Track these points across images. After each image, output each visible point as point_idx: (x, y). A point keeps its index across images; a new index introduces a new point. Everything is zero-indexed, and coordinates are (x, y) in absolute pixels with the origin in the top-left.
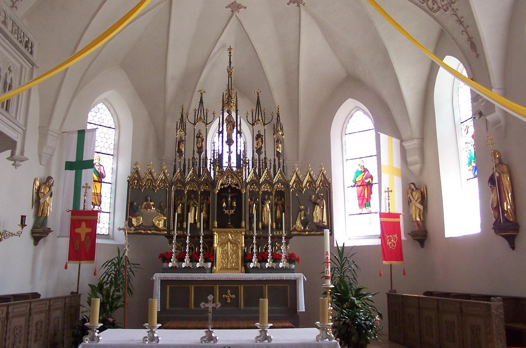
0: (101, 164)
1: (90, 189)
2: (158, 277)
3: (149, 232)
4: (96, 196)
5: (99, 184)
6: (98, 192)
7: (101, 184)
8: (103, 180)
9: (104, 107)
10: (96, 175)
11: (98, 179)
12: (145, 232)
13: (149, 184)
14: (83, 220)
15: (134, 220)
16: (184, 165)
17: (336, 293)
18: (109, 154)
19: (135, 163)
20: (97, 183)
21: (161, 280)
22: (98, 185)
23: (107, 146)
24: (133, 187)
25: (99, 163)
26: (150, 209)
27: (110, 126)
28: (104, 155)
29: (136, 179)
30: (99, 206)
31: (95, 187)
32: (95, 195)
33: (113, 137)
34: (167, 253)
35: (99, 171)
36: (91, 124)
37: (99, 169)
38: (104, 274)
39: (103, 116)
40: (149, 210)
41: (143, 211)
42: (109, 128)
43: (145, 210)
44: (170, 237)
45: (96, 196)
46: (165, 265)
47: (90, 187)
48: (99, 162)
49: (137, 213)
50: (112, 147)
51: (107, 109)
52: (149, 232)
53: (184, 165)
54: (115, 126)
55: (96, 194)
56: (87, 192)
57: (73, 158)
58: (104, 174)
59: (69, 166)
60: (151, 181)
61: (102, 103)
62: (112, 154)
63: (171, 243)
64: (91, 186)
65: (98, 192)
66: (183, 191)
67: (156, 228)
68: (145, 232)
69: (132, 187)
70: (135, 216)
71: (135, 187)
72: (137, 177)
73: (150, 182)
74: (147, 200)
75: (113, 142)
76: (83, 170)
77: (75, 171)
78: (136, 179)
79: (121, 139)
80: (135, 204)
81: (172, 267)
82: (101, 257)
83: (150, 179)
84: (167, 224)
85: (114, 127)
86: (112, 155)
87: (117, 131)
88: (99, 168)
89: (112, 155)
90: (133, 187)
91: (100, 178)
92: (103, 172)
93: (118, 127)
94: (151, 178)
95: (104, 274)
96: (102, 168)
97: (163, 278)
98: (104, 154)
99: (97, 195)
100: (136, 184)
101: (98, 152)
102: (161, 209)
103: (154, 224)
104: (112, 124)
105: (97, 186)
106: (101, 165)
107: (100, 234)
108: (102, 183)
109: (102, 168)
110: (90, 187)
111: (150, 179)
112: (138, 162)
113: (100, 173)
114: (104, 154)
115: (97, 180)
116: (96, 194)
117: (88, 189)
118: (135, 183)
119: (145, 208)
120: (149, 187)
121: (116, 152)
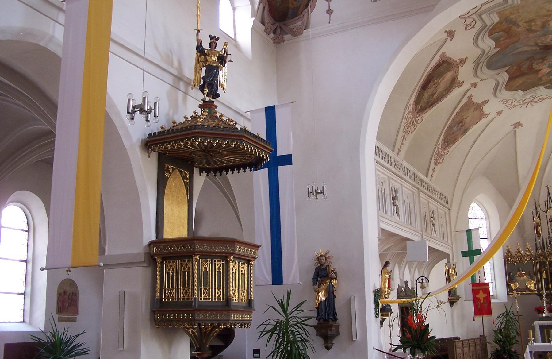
2: (537, 324)
13: (519, 259)
14: (480, 289)
15: (512, 286)
16: (543, 243)
34: (540, 307)
40: (522, 277)
44: (541, 296)
46: (540, 315)
49: (514, 280)
50: (486, 232)
52: (525, 293)
53: (543, 243)
57: (282, 170)
59: (464, 254)
63: (542, 299)
66: (545, 263)
67: (529, 290)
68: (522, 293)
71: (509, 262)
73: (519, 258)
74: (519, 271)
80: (511, 274)
81: (545, 317)
82: (496, 312)
84: (537, 286)
86: (487, 239)
87: (488, 220)
89: (487, 239)
93: (487, 218)
94: (520, 255)
102: (530, 276)
103: (527, 287)
119: (519, 276)
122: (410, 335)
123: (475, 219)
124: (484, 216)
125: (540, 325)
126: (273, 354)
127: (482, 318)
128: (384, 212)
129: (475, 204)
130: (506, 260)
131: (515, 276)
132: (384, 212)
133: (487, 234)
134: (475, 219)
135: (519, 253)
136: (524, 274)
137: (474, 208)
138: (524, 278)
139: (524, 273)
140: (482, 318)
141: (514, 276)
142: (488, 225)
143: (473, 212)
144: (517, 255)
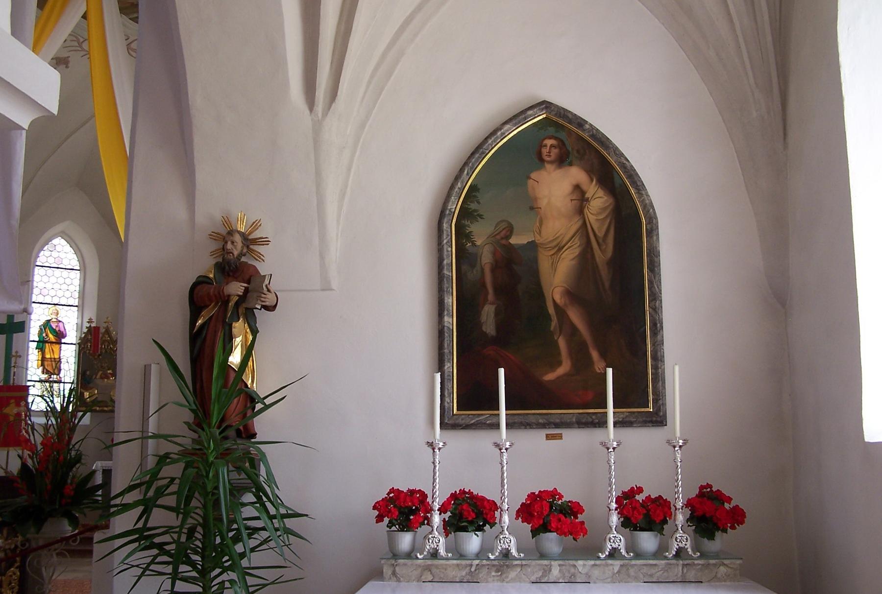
0: (60, 319)
1: (22, 358)
3: (106, 409)
4: (53, 362)
5: (58, 346)
6: (56, 357)
7: (59, 347)
8: (63, 341)
9: (63, 242)
10: (53, 335)
11: (56, 340)
12: (101, 409)
13: (106, 347)
14: (12, 398)
17: (262, 493)
18: (71, 304)
19: (88, 321)
20: (54, 344)
21: (103, 470)
22: (56, 347)
23: (68, 294)
24: (85, 352)
25: (57, 319)
26: (107, 379)
27: (72, 268)
28: (64, 306)
29: (89, 341)
30: (58, 374)
31: (51, 350)
32: (52, 361)
33: (77, 282)
35: (57, 329)
36: (44, 268)
37: (57, 326)
38: (137, 470)
39: (62, 255)
40: (106, 380)
41: (99, 381)
42: (71, 271)
43: (101, 380)
45: (53, 362)
47: (20, 356)
48: (56, 317)
49: (91, 385)
50: (77, 295)
51: (68, 244)
52: (98, 408)
54: (80, 266)
55: (53, 360)
56: (17, 362)
58: (64, 333)
60: (108, 342)
61: (60, 238)
62: (75, 305)
64: (22, 355)
65: (57, 356)
68: (101, 409)
69: (84, 352)
70: (87, 390)
71: (88, 351)
72: (91, 339)
73: (106, 344)
75: (77, 289)
76: (14, 335)
77: (5, 335)
78: (89, 341)
79: (87, 285)
80: (88, 373)
83: (107, 341)
85: (79, 269)
86: (76, 306)
87: (83, 273)
88: (56, 324)
89: (76, 306)
90: (85, 352)
91: (59, 338)
92: (62, 329)
93: (83, 269)
94: (109, 338)
95: (137, 470)
96: (61, 324)
97: (106, 467)
98: (64, 305)
99: (55, 361)
100: (89, 347)
101: (56, 303)
104: (75, 263)
105: (54, 349)
106: (60, 321)
107: (37, 411)
108: (62, 345)
109: (61, 324)
110: (20, 356)
111: (107, 341)
112: (92, 318)
113: (59, 332)
114: (64, 305)
115: (54, 341)
116: (53, 360)
117: (18, 358)
118: (87, 346)
119: (102, 378)
120: (106, 351)
121: (81, 303)
122: (682, 503)
123: (58, 268)
124: (79, 265)
125: (104, 468)
126: (167, 529)
127: (8, 452)
128: (268, 244)
129: (63, 240)
130: (83, 346)
131: (94, 376)
132: (268, 244)
133: (79, 298)
134: (58, 268)
135: (107, 336)
136: (110, 373)
137: (58, 248)
138: (109, 382)
139: (111, 372)
140: (8, 452)
141: (92, 377)
142: (82, 283)
143: (55, 254)
144: (104, 339)
